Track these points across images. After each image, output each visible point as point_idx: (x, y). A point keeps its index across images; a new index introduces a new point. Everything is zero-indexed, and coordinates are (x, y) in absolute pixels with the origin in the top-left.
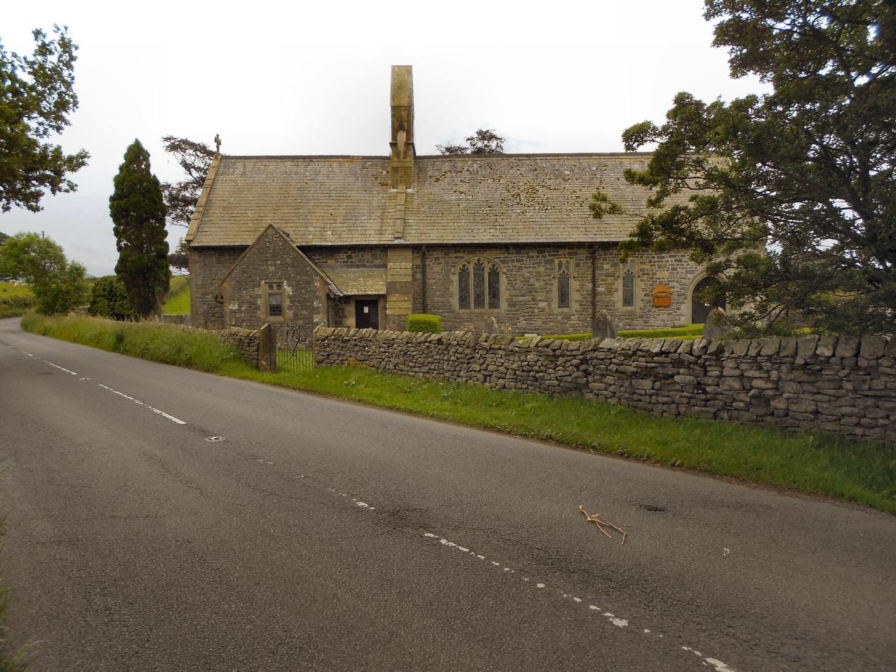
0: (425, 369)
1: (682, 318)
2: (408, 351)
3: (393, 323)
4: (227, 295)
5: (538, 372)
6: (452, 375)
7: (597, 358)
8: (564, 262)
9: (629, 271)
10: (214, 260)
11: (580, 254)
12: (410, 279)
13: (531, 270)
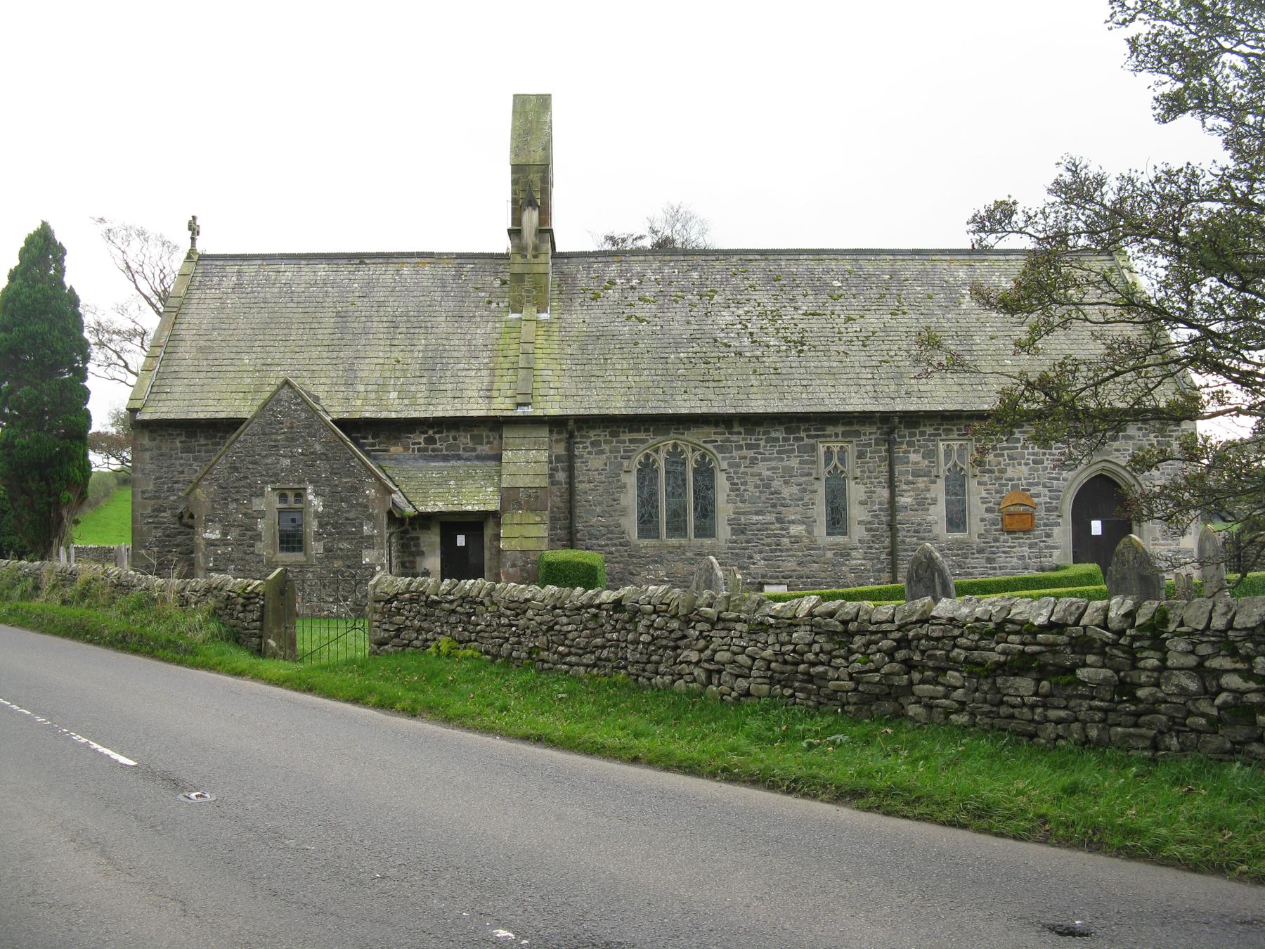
0: (589, 659)
1: (1056, 553)
2: (556, 623)
3: (514, 565)
4: (202, 513)
5: (813, 664)
6: (644, 670)
7: (928, 637)
8: (836, 450)
9: (955, 465)
10: (179, 445)
11: (865, 434)
12: (544, 482)
13: (773, 464)
